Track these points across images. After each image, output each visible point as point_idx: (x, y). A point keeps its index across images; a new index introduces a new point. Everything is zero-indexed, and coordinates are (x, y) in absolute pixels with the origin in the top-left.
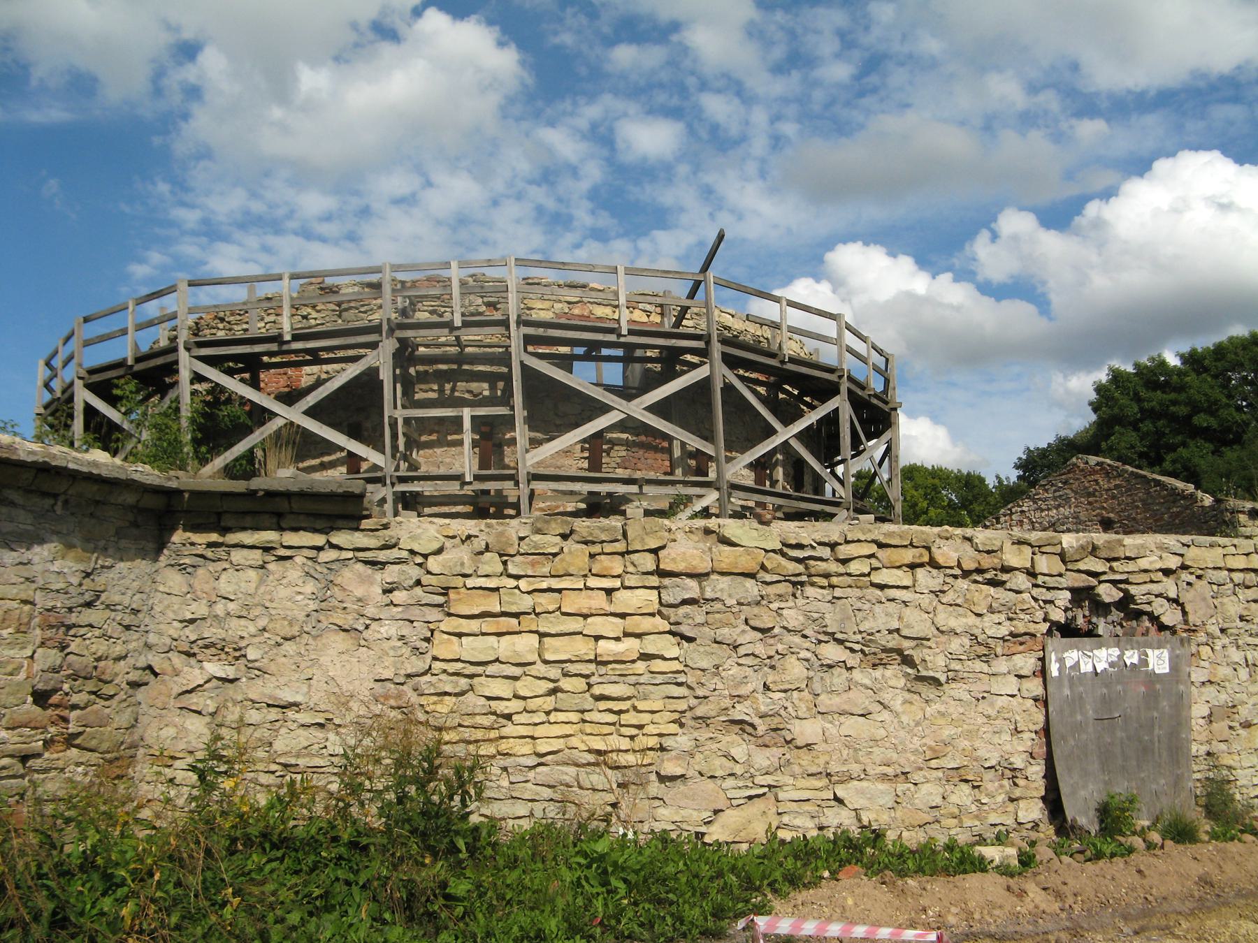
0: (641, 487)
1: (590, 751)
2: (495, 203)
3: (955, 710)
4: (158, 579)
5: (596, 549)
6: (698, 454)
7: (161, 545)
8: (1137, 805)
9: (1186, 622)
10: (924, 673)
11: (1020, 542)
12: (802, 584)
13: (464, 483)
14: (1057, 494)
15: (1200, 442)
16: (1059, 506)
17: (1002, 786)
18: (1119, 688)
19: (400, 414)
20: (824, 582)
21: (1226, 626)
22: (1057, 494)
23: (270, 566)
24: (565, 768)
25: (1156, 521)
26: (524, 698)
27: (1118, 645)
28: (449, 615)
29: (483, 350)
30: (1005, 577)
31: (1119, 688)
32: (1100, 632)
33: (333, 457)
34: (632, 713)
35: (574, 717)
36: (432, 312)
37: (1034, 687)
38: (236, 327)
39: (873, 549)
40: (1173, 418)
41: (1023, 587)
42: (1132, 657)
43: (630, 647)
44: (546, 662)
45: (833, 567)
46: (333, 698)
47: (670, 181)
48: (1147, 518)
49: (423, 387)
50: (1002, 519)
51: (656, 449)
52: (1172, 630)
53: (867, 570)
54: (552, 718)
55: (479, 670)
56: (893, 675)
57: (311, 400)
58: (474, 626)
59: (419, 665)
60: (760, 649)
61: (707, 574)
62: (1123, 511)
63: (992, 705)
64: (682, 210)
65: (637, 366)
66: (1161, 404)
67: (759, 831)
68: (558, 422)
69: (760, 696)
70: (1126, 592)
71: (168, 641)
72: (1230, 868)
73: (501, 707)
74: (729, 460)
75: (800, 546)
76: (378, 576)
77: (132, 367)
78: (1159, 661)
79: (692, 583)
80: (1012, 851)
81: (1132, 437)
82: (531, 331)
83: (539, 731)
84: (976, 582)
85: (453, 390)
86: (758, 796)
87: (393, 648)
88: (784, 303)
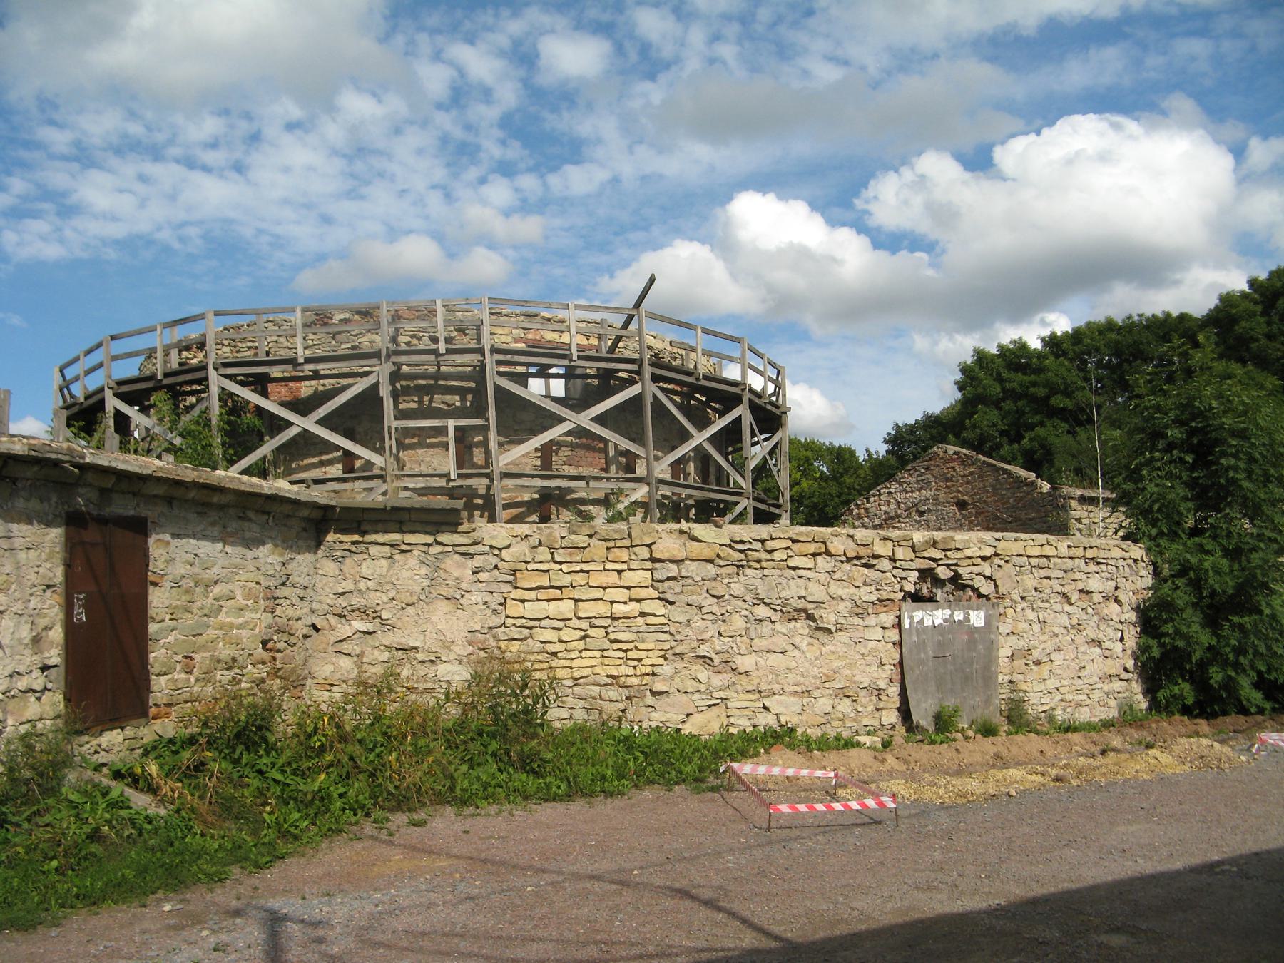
0: (588, 483)
1: (607, 676)
2: (398, 131)
3: (841, 649)
4: (318, 566)
5: (611, 544)
6: (627, 453)
7: (319, 544)
8: (960, 713)
9: (997, 592)
10: (821, 625)
11: (885, 539)
12: (743, 566)
13: (449, 480)
14: (920, 478)
15: (1057, 422)
16: (922, 488)
17: (871, 700)
18: (950, 636)
19: (396, 424)
20: (758, 565)
21: (1024, 595)
22: (920, 478)
23: (394, 557)
24: (592, 687)
25: (1003, 504)
26: (565, 642)
27: (950, 608)
28: (516, 588)
29: (460, 368)
30: (874, 562)
31: (950, 636)
32: (938, 599)
33: (331, 456)
34: (635, 651)
35: (598, 654)
36: (412, 337)
37: (893, 635)
38: (240, 344)
39: (789, 543)
40: (1033, 399)
41: (886, 569)
42: (959, 616)
43: (633, 608)
44: (579, 618)
45: (764, 556)
46: (440, 643)
47: (590, 107)
48: (995, 501)
49: (406, 398)
50: (872, 499)
51: (594, 449)
52: (987, 597)
53: (784, 558)
54: (583, 654)
55: (536, 623)
56: (801, 626)
57: (323, 411)
58: (532, 595)
59: (497, 621)
60: (716, 609)
61: (683, 561)
62: (975, 494)
63: (865, 647)
64: (599, 141)
65: (579, 382)
66: (1021, 385)
67: (715, 727)
68: (516, 428)
69: (715, 640)
70: (956, 572)
71: (326, 607)
72: (1014, 750)
73: (550, 648)
74: (657, 458)
75: (742, 542)
76: (469, 563)
77: (161, 381)
78: (977, 618)
79: (673, 566)
80: (878, 739)
81: (994, 415)
82: (501, 357)
83: (575, 663)
84: (855, 565)
85: (431, 401)
86: (715, 705)
87: (480, 610)
88: (700, 331)
